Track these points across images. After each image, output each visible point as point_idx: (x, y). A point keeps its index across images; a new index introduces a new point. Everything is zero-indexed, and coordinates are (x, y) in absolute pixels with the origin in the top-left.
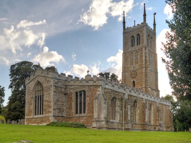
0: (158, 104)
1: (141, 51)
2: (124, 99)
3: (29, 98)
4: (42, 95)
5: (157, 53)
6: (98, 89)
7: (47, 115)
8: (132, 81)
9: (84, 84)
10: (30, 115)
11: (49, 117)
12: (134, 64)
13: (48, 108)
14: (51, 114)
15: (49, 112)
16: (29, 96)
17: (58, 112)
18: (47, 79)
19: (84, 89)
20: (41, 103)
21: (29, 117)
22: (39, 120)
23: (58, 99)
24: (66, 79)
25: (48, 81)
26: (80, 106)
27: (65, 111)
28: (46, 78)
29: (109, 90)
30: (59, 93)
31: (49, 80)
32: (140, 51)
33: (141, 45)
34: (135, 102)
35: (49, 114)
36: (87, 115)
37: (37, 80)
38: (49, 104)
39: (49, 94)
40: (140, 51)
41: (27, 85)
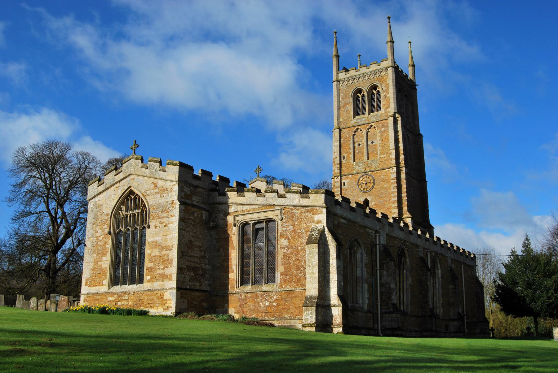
0: (449, 261)
1: (383, 126)
2: (378, 246)
3: (98, 234)
5: (421, 132)
7: (156, 285)
9: (271, 202)
10: (100, 284)
11: (163, 290)
14: (170, 282)
15: (164, 277)
16: (97, 228)
17: (191, 279)
18: (160, 183)
21: (93, 290)
22: (128, 300)
23: (190, 241)
24: (214, 186)
27: (207, 276)
28: (156, 181)
29: (343, 221)
30: (193, 225)
33: (383, 111)
34: (401, 254)
37: (126, 187)
38: (165, 255)
39: (166, 226)
41: (91, 199)
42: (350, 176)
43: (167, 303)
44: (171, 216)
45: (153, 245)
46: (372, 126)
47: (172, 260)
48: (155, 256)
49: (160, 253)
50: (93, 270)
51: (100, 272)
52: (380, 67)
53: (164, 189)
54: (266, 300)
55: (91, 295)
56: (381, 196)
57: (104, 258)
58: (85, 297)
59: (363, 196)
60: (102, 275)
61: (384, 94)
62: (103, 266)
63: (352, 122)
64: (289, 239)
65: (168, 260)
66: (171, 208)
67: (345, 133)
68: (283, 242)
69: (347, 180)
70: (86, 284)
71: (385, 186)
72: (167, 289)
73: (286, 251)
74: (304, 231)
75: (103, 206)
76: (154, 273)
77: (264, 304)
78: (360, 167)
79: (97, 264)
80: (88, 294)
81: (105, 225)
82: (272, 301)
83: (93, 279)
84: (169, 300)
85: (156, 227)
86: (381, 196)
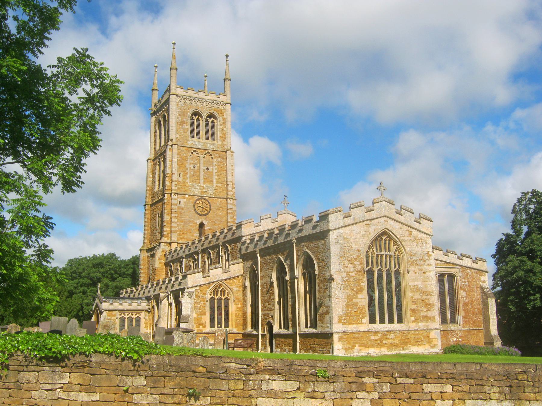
3: (347, 270)
4: (393, 270)
6: (482, 278)
8: (199, 222)
11: (428, 330)
12: (202, 181)
13: (425, 310)
14: (434, 323)
18: (414, 232)
19: (452, 271)
20: (390, 291)
25: (418, 241)
26: (379, 296)
28: (410, 229)
31: (419, 237)
32: (217, 155)
35: (427, 324)
36: (463, 329)
39: (424, 273)
40: (217, 155)
42: (187, 196)
43: (433, 341)
44: (429, 265)
45: (414, 289)
46: (208, 153)
47: (433, 305)
48: (417, 299)
49: (422, 297)
50: (347, 307)
51: (357, 310)
52: (218, 99)
53: (419, 239)
54: (454, 337)
55: (348, 333)
56: (216, 222)
57: (360, 296)
58: (341, 335)
59: (199, 219)
60: (360, 313)
61: (222, 127)
62: (360, 304)
63: (189, 143)
64: (466, 291)
65: (430, 304)
66: (427, 258)
67: (182, 151)
68: (462, 293)
69: (183, 199)
70: (340, 321)
71: (220, 214)
72: (432, 330)
73: (465, 300)
74: (475, 287)
75: (352, 241)
76: (417, 315)
77: (453, 340)
78: (197, 190)
79: (351, 300)
80: (344, 332)
81: (356, 261)
82: (458, 337)
83: (348, 316)
84: (435, 339)
85: (415, 273)
86: (216, 222)
